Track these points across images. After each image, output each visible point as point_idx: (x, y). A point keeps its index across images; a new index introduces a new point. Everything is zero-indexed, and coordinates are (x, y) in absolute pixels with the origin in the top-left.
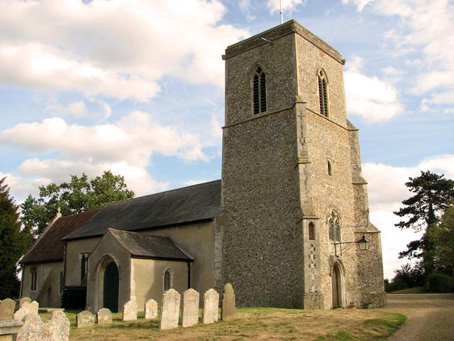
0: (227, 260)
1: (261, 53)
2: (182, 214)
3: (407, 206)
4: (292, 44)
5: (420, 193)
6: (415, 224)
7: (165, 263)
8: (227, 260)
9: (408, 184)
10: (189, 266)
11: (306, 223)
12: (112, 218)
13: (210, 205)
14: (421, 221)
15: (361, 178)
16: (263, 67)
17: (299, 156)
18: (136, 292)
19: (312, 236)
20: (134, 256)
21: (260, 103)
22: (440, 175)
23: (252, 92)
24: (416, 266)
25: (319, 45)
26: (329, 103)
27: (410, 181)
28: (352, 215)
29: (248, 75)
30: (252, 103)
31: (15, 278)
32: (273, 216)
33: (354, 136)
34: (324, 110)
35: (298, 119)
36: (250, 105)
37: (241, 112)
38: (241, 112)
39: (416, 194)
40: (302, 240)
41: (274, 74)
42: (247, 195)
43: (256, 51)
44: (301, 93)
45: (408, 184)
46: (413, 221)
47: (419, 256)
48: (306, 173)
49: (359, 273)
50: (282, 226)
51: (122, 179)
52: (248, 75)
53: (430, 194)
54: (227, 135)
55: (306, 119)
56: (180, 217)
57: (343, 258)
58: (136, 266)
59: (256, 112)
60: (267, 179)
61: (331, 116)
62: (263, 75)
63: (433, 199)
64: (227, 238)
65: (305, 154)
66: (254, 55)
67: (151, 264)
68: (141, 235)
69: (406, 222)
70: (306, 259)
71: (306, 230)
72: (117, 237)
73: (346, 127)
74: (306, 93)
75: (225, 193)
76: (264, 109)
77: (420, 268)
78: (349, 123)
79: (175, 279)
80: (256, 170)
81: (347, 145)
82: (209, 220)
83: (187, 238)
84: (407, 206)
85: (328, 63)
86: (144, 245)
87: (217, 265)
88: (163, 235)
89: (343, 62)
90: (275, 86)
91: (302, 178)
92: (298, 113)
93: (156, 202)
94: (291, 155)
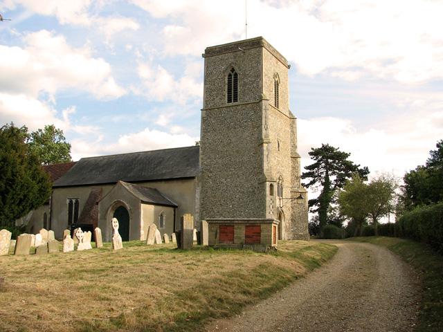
0: (203, 208)
1: (235, 57)
2: (165, 172)
3: (308, 171)
4: (260, 55)
5: (319, 161)
6: (314, 186)
7: (160, 208)
8: (203, 208)
9: (311, 154)
10: (175, 211)
11: (268, 184)
12: (94, 172)
13: (187, 166)
14: (318, 184)
15: (296, 153)
16: (236, 68)
17: (263, 137)
18: (144, 227)
19: (272, 194)
20: (143, 202)
21: (233, 95)
22: (336, 148)
23: (227, 86)
24: (312, 220)
25: (275, 54)
26: (280, 97)
27: (312, 151)
28: (289, 179)
29: (224, 73)
30: (226, 95)
31: (326, 214)
32: (241, 178)
33: (294, 122)
34: (277, 104)
35: (264, 112)
36: (224, 96)
37: (217, 100)
38: (217, 100)
39: (316, 162)
40: (265, 196)
41: (245, 75)
42: (220, 161)
43: (231, 55)
44: (265, 92)
45: (311, 154)
46: (312, 183)
47: (315, 211)
48: (268, 150)
49: (292, 220)
50: (247, 185)
51: (61, 132)
52: (224, 73)
53: (327, 163)
54: (205, 116)
55: (268, 112)
56: (164, 174)
57: (284, 209)
58: (144, 209)
59: (229, 101)
60: (237, 151)
61: (281, 108)
62: (236, 74)
63: (329, 167)
64: (204, 192)
65: (267, 136)
66: (230, 59)
67: (152, 207)
68: (139, 185)
69: (306, 184)
70: (267, 208)
71: (268, 189)
72: (127, 187)
73: (288, 115)
74: (267, 92)
75: (202, 159)
76: (236, 100)
77: (316, 221)
78: (290, 113)
79: (166, 220)
80: (229, 144)
81: (288, 129)
82: (193, 178)
83: (173, 191)
84: (308, 171)
85: (281, 69)
86: (145, 194)
87: (197, 210)
88: (151, 187)
89: (289, 67)
90: (245, 84)
91: (265, 153)
92: (264, 107)
93: (135, 160)
94: (256, 136)
